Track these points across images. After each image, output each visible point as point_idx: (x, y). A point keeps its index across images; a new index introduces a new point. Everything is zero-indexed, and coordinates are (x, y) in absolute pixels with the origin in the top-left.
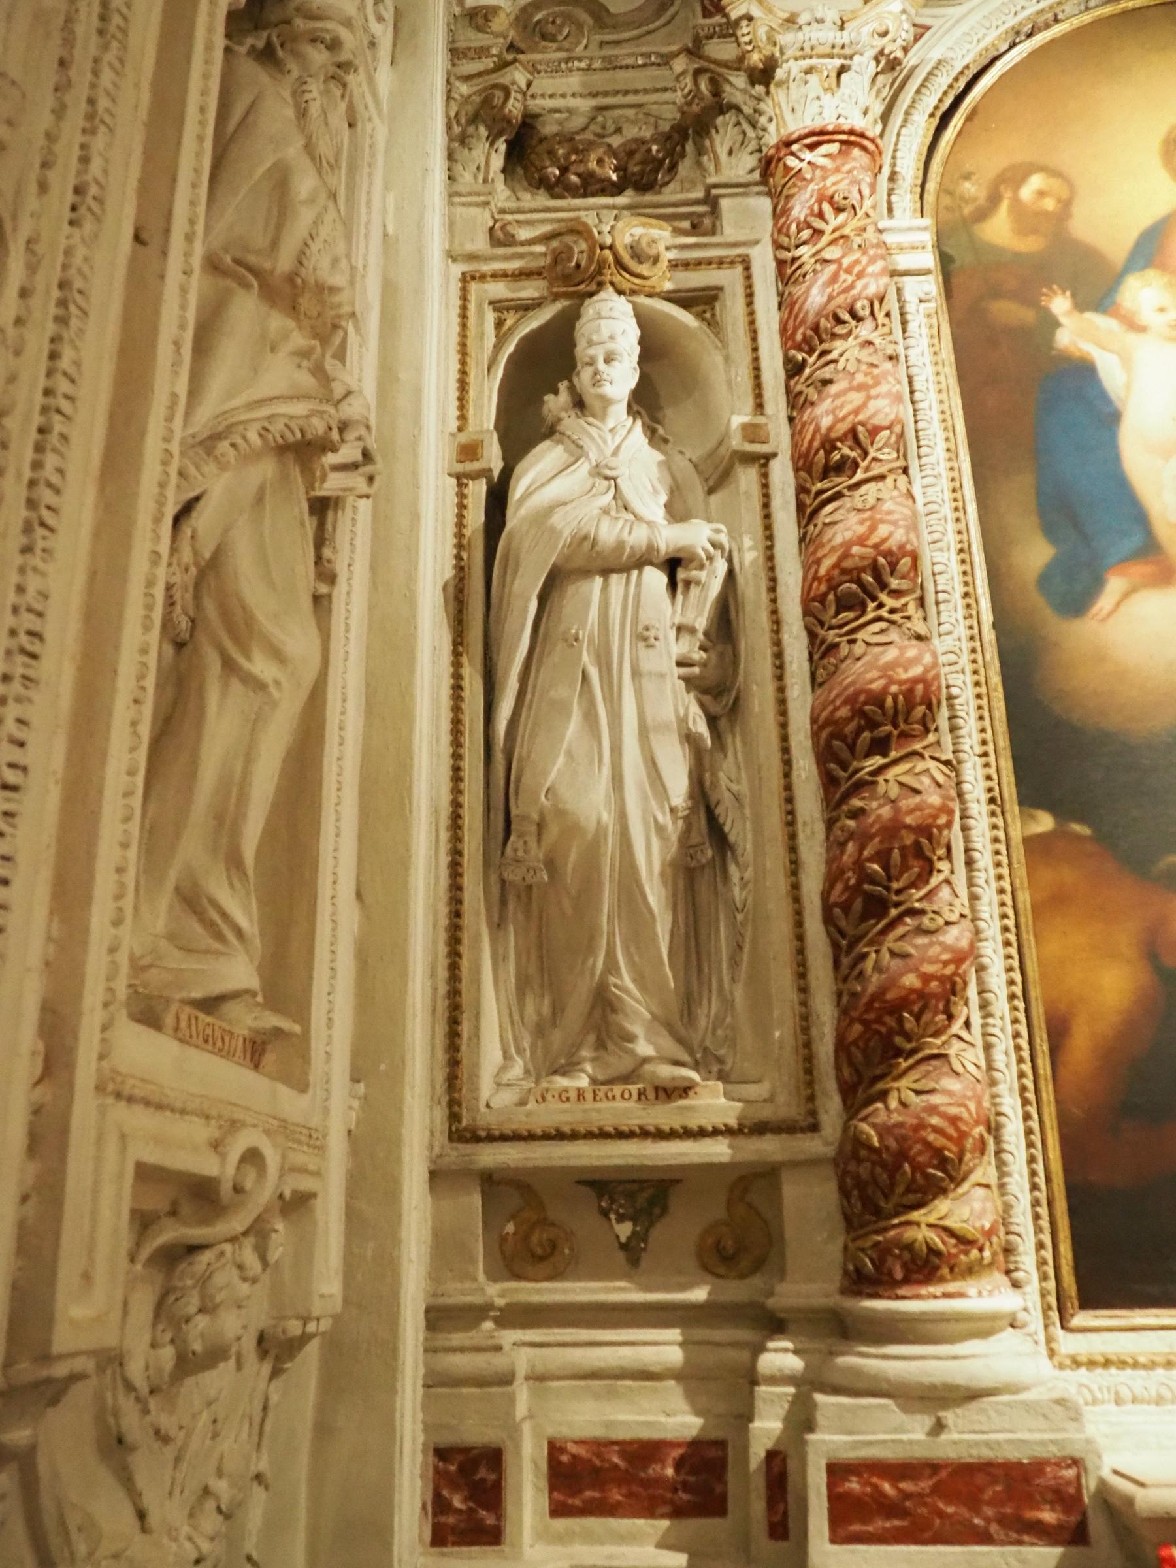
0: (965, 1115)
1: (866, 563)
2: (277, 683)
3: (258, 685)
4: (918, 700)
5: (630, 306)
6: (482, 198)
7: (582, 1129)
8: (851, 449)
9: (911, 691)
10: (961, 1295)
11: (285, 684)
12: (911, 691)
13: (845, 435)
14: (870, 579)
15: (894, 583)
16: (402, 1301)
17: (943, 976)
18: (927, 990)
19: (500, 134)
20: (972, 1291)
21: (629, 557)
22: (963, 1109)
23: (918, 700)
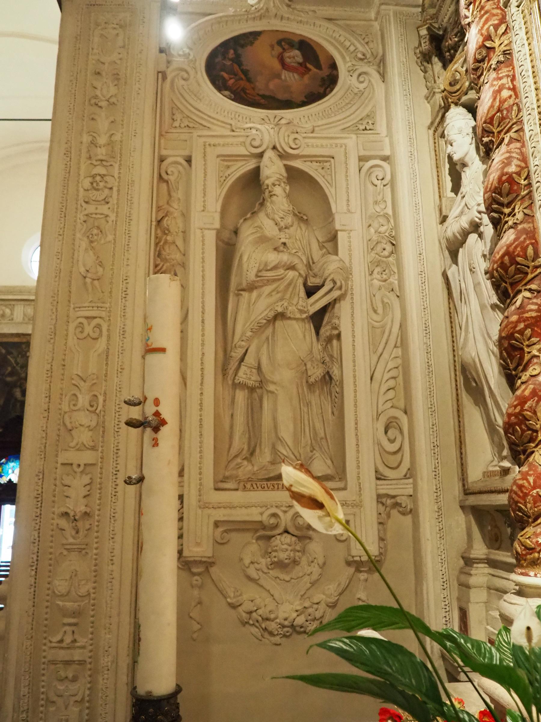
0: (526, 484)
1: (490, 201)
2: (276, 390)
3: (272, 392)
4: (508, 265)
5: (461, 108)
6: (432, 94)
7: (144, 519)
8: (488, 136)
9: (502, 263)
10: (527, 575)
11: (278, 389)
12: (502, 263)
13: (482, 133)
14: (496, 206)
15: (505, 200)
16: (423, 554)
17: (515, 413)
18: (511, 422)
19: (430, 58)
20: (532, 573)
21: (461, 236)
22: (525, 481)
23: (508, 265)
